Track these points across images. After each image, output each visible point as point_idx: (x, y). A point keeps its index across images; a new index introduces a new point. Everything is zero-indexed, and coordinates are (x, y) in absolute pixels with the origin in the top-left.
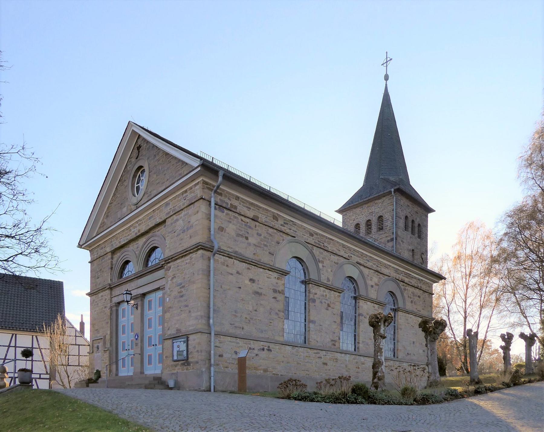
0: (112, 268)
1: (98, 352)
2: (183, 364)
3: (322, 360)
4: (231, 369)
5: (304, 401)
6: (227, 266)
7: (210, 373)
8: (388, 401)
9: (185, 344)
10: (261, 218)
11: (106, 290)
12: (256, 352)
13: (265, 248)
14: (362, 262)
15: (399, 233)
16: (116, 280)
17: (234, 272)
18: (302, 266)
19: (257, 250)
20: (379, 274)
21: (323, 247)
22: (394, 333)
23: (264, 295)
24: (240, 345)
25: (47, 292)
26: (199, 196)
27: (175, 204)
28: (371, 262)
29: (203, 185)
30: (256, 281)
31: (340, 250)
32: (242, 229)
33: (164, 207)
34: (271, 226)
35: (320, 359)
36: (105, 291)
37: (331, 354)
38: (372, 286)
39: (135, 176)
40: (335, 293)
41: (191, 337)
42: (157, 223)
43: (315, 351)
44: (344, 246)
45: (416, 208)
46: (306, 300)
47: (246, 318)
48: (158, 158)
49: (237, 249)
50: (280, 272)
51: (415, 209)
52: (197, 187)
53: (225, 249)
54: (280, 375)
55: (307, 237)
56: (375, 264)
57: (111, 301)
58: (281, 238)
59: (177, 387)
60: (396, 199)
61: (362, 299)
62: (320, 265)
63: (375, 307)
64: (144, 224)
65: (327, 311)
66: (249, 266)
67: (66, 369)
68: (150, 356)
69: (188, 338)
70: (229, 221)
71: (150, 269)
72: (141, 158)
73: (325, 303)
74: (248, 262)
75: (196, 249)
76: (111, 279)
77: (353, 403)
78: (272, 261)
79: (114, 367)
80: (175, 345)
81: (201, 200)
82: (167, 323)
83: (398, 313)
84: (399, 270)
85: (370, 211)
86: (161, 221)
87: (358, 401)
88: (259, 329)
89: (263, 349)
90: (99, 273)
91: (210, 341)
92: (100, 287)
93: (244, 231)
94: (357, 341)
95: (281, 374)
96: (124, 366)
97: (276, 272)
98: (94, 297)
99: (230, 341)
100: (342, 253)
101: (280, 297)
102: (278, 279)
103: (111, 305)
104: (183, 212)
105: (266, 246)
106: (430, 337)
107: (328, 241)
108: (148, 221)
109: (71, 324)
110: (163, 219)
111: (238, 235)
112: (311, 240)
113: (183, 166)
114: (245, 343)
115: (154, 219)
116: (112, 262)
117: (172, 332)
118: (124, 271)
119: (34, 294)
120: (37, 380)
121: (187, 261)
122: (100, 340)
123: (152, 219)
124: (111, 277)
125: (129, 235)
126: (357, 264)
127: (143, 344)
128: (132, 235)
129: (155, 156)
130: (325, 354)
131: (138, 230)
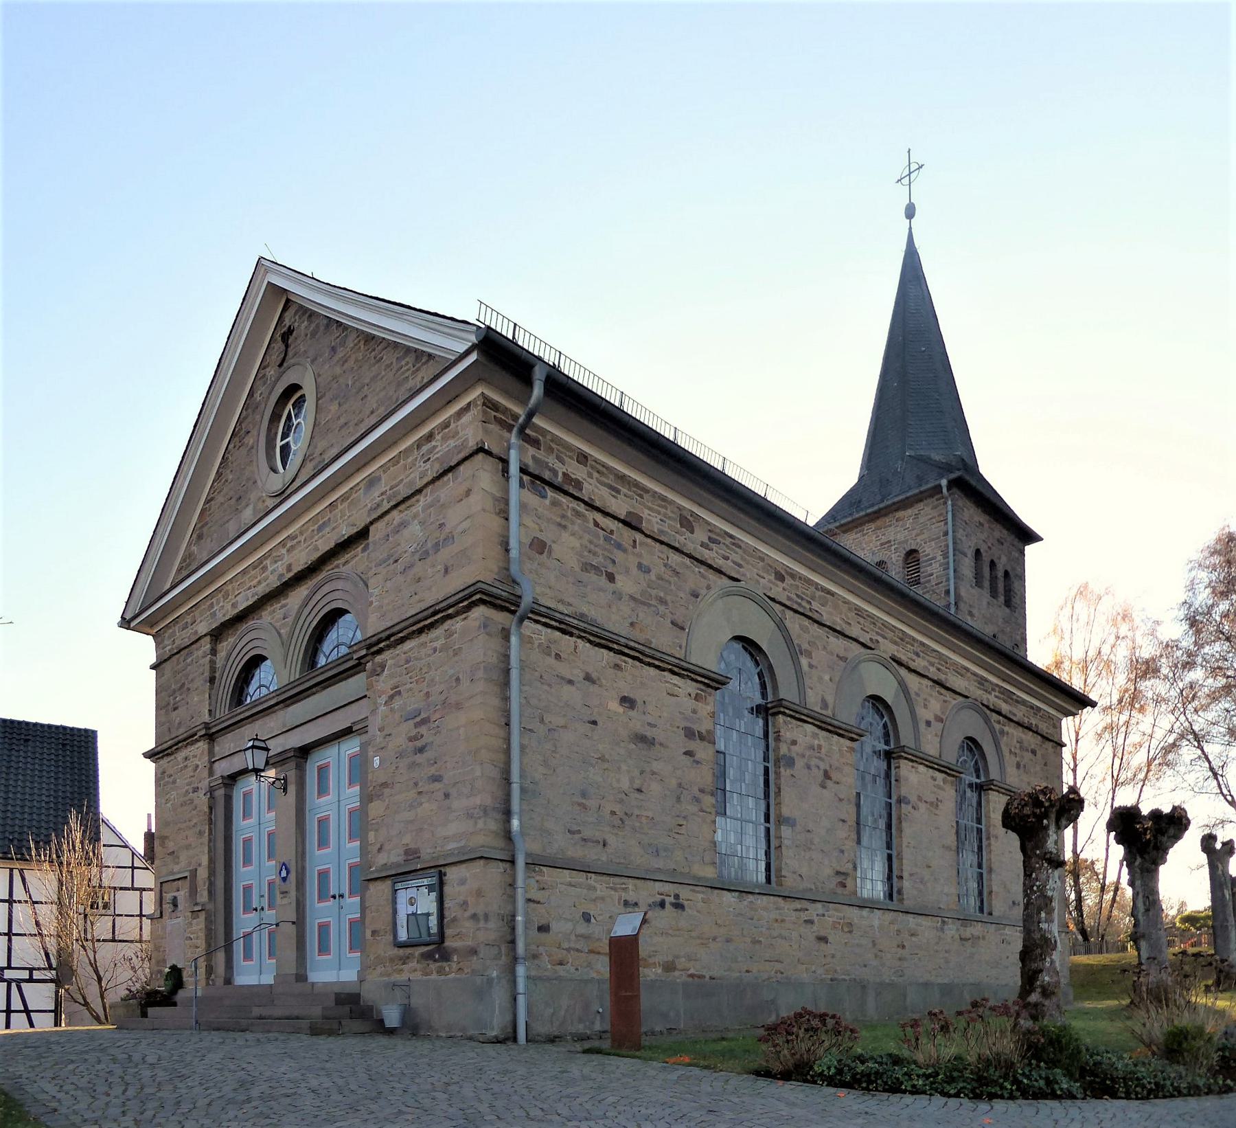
0: (212, 680)
1: (174, 914)
2: (428, 956)
3: (815, 928)
4: (572, 970)
5: (863, 1089)
6: (558, 657)
7: (514, 982)
8: (1157, 1084)
9: (433, 895)
10: (649, 521)
11: (197, 741)
13: (662, 608)
14: (904, 658)
15: (963, 593)
16: (223, 712)
17: (578, 675)
18: (757, 664)
19: (640, 614)
20: (943, 691)
22: (980, 848)
23: (661, 744)
25: (53, 757)
26: (472, 444)
27: (395, 478)
28: (923, 658)
29: (485, 412)
30: (639, 702)
31: (850, 624)
32: (597, 549)
33: (361, 491)
34: (677, 545)
35: (809, 926)
36: (192, 743)
37: (836, 910)
38: (928, 723)
39: (275, 417)
40: (842, 740)
41: (452, 874)
42: (343, 539)
43: (798, 905)
44: (859, 612)
45: (999, 532)
46: (766, 759)
47: (613, 813)
48: (341, 355)
49: (584, 609)
50: (703, 680)
51: (997, 534)
52: (466, 418)
53: (552, 606)
54: (708, 977)
55: (770, 581)
56: (932, 664)
57: (211, 773)
58: (704, 583)
59: (412, 1027)
60: (952, 506)
61: (906, 758)
62: (804, 661)
63: (935, 780)
64: (303, 545)
65: (824, 791)
66: (618, 659)
67: (92, 959)
68: (324, 929)
69: (441, 875)
70: (560, 525)
71: (322, 673)
72: (292, 361)
73: (818, 767)
74: (615, 646)
75: (465, 603)
76: (210, 711)
77: (1039, 1095)
78: (680, 647)
79: (220, 957)
80: (403, 897)
81: (481, 456)
82: (377, 830)
83: (988, 794)
84: (986, 680)
85: (884, 539)
86: (355, 531)
87: (1056, 1087)
88: (650, 845)
89: (662, 905)
90: (177, 694)
91: (512, 885)
92: (181, 732)
93: (603, 554)
94: (895, 872)
95: (711, 973)
96: (248, 956)
97: (692, 679)
98: (164, 762)
99: (570, 885)
100: (855, 631)
101: (704, 752)
102: (697, 698)
104: (421, 498)
105: (662, 601)
106: (1142, 857)
107: (820, 597)
108: (316, 537)
109: (119, 836)
110: (360, 525)
111: (587, 567)
112: (778, 591)
113: (418, 366)
114: (611, 888)
115: (334, 529)
116: (212, 662)
117: (392, 857)
118: (248, 687)
120: (23, 985)
121: (437, 644)
122: (180, 882)
123: (328, 529)
124: (210, 705)
125: (259, 583)
126: (894, 663)
127: (304, 895)
128: (268, 581)
129: (334, 349)
130: (821, 912)
131: (285, 566)
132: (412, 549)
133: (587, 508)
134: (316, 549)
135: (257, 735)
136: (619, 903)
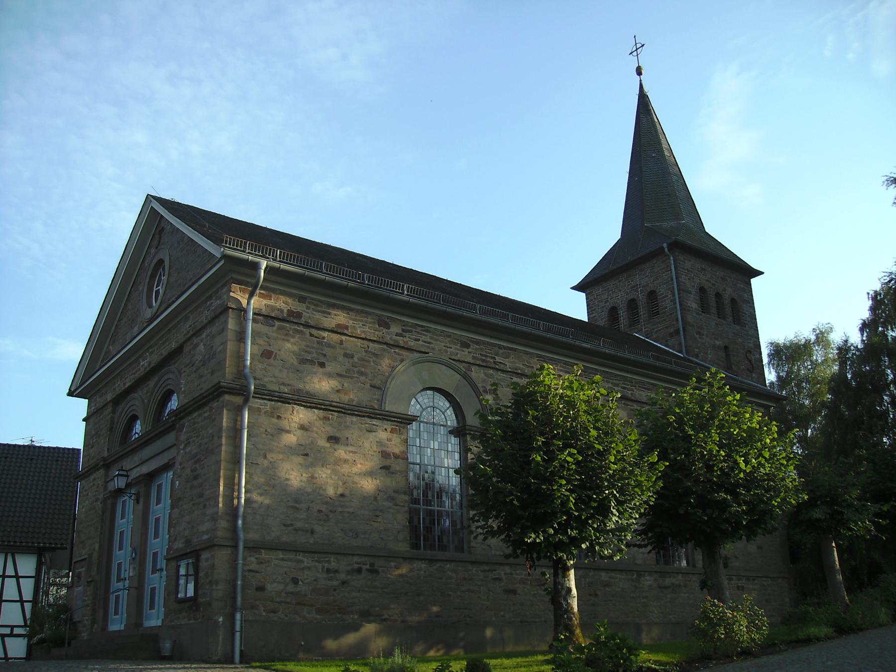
0: (111, 430)
3: (503, 584)
12: (343, 576)
13: (363, 378)
21: (493, 365)
24: (306, 564)
27: (196, 318)
39: (153, 276)
47: (320, 511)
57: (105, 488)
72: (162, 247)
74: (323, 407)
76: (108, 449)
89: (359, 571)
97: (387, 420)
99: (282, 559)
103: (104, 495)
105: (362, 374)
107: (503, 353)
111: (303, 361)
116: (112, 418)
119: (30, 471)
123: (167, 344)
132: (200, 359)
133: (305, 327)
134: (162, 354)
135: (122, 467)
136: (322, 570)
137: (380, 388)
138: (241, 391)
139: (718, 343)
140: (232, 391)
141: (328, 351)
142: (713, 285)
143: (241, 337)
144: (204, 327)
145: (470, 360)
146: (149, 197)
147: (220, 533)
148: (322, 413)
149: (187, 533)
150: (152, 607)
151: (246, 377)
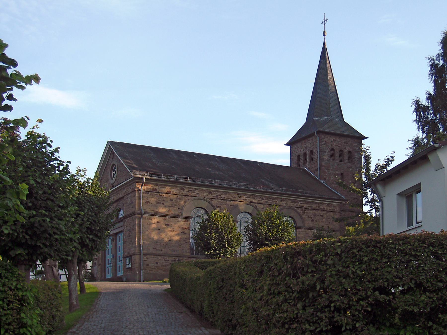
39: (112, 168)
56: (269, 200)
79: (104, 274)
105: (176, 205)
111: (158, 203)
137: (181, 209)
138: (140, 213)
139: (337, 172)
140: (138, 214)
141: (165, 199)
142: (339, 146)
143: (140, 198)
144: (129, 194)
145: (212, 197)
146: (110, 143)
147: (137, 251)
148: (163, 218)
149: (128, 251)
150: (119, 271)
151: (141, 209)
